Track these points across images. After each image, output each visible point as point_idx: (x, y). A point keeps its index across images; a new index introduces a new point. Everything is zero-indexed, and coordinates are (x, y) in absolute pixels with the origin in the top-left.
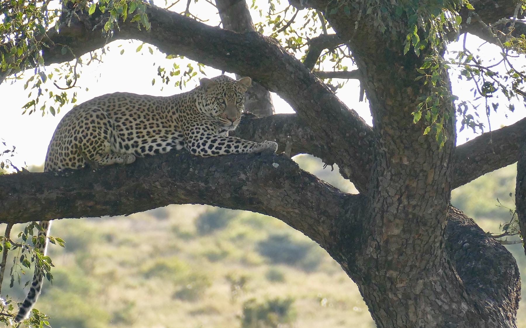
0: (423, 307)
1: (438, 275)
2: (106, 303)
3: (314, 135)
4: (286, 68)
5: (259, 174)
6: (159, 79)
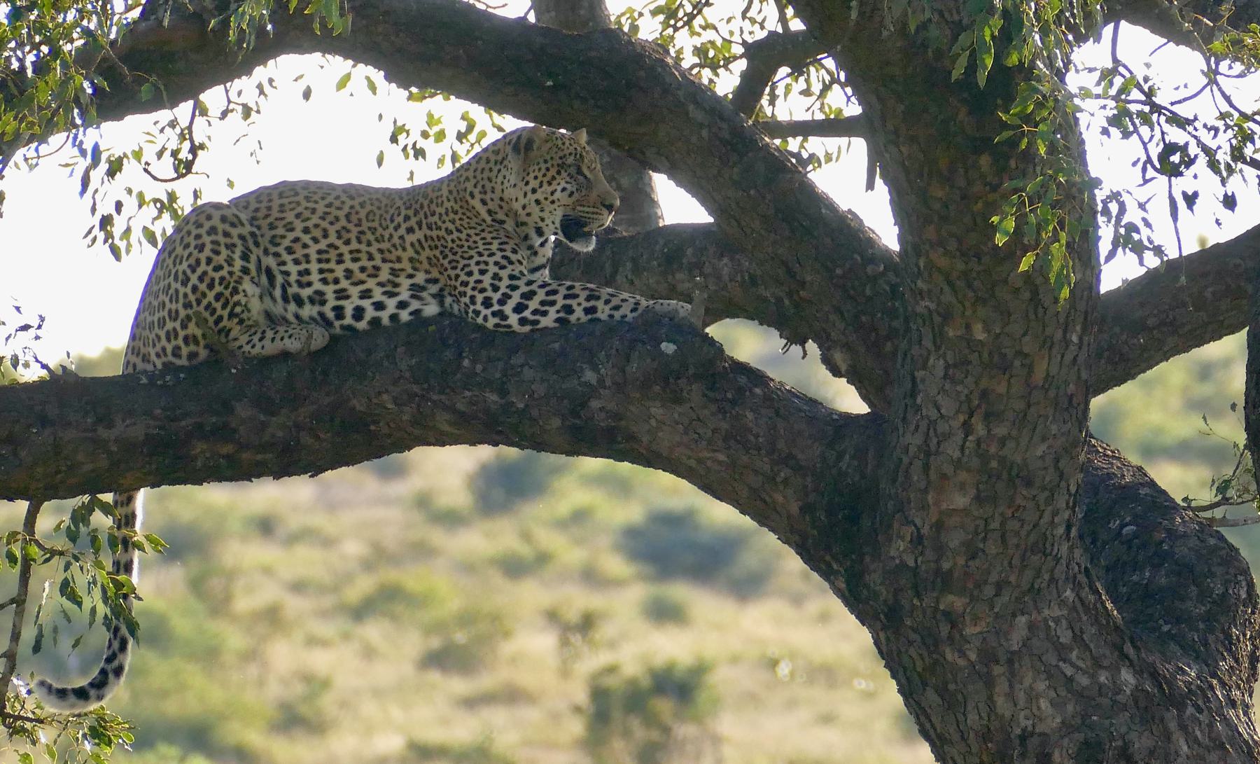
0: (1028, 681)
1: (1062, 603)
2: (261, 683)
3: (759, 273)
4: (687, 114)
5: (628, 369)
6: (393, 152)
